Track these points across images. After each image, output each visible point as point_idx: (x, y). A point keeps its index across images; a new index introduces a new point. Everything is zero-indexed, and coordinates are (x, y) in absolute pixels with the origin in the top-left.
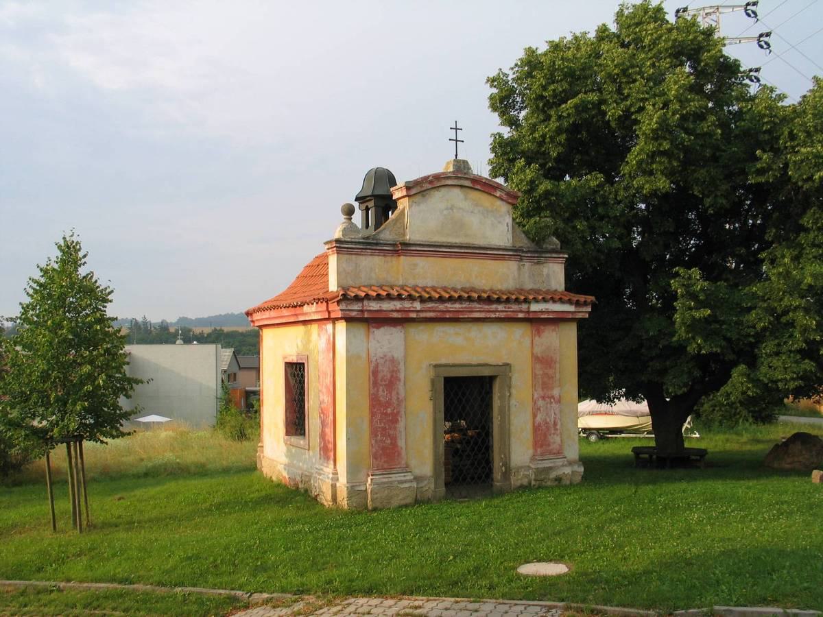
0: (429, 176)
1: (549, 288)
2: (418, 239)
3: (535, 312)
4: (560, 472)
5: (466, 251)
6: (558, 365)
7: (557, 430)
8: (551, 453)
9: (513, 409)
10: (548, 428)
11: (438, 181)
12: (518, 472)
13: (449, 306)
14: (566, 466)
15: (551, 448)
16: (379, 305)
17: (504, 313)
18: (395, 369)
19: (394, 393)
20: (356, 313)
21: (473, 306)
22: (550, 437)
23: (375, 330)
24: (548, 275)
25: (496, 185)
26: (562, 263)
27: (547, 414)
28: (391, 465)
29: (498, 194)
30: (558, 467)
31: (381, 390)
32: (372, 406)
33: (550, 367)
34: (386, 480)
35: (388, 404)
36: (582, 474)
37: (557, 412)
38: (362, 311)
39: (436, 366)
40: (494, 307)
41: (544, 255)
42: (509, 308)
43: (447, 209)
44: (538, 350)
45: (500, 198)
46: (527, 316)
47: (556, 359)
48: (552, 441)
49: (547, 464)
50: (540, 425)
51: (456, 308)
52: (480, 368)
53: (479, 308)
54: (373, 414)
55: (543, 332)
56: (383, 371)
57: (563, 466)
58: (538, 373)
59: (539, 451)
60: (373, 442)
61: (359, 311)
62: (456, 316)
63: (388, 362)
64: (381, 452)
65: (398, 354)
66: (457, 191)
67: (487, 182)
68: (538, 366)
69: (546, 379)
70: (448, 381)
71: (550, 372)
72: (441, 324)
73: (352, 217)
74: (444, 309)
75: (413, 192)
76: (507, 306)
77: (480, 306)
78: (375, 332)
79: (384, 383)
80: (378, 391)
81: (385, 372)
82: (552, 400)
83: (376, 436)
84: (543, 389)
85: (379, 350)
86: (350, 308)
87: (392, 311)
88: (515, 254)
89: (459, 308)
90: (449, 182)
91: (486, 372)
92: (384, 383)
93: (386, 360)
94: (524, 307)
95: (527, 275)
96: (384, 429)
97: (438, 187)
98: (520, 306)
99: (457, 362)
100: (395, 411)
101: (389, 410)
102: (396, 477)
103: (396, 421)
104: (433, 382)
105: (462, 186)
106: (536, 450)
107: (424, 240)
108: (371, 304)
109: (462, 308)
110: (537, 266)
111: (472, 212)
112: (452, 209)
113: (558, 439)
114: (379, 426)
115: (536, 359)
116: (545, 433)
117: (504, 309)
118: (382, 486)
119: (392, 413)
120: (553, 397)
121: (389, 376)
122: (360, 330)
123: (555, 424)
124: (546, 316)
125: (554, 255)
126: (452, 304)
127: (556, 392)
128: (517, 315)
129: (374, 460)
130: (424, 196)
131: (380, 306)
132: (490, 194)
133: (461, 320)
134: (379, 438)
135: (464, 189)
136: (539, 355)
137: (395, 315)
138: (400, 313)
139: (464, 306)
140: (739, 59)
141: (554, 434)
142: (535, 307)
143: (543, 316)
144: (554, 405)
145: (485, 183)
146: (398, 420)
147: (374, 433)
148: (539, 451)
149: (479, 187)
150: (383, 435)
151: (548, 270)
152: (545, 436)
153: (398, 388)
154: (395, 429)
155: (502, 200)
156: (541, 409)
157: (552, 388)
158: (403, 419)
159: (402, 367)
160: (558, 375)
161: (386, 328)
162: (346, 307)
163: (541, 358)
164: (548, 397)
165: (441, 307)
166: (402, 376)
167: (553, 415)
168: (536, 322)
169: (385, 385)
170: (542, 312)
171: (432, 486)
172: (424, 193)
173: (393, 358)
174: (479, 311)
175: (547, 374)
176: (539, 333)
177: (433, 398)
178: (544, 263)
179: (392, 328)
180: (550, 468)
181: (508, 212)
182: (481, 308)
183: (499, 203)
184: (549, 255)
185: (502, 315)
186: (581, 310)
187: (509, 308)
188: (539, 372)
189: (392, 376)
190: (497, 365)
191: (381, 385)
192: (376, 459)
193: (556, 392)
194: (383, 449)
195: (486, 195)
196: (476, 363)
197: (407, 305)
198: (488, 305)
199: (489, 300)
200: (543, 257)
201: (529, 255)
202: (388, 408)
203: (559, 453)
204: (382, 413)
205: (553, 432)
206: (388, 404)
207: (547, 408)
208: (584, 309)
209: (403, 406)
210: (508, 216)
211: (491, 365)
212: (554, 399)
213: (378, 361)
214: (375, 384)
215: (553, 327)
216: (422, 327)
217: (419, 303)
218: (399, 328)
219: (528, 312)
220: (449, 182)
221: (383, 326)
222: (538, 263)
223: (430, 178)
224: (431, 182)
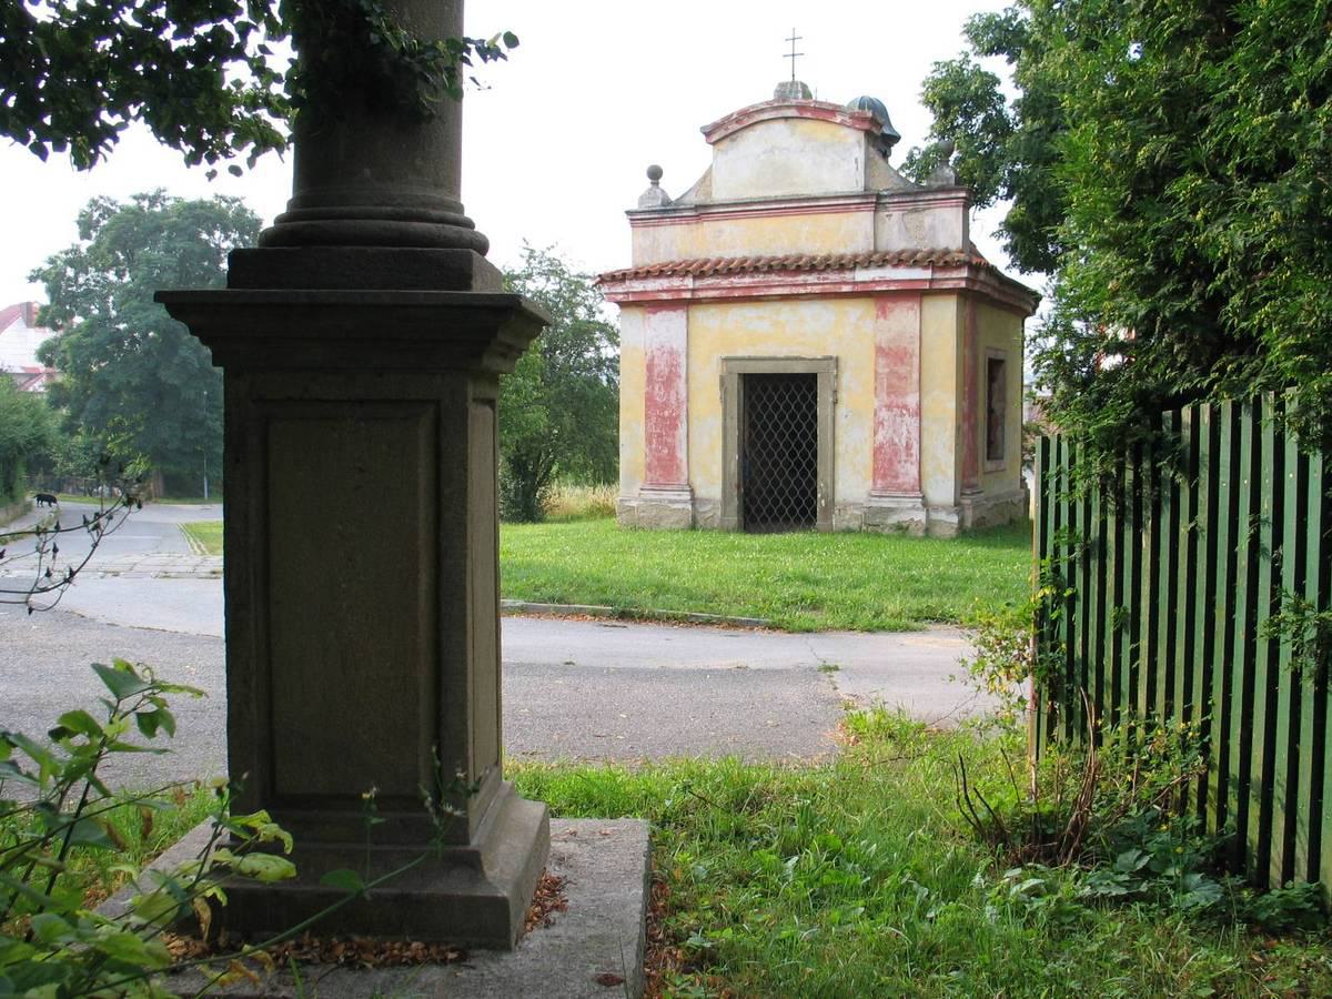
0: (732, 115)
1: (935, 246)
2: (723, 197)
4: (904, 517)
5: (788, 205)
8: (899, 488)
9: (841, 421)
12: (845, 510)
13: (736, 281)
14: (918, 509)
15: (900, 481)
17: (820, 287)
19: (673, 392)
20: (622, 296)
22: (899, 466)
23: (651, 315)
24: (932, 227)
26: (957, 206)
27: (894, 431)
29: (838, 119)
30: (902, 510)
31: (657, 389)
34: (656, 497)
35: (666, 405)
36: (956, 526)
39: (726, 360)
40: (801, 279)
41: (921, 198)
42: (824, 279)
43: (764, 153)
45: (842, 124)
49: (886, 503)
50: (881, 446)
54: (648, 417)
57: (913, 508)
58: (880, 371)
61: (623, 293)
62: (747, 293)
65: (679, 344)
66: (780, 126)
68: (882, 361)
69: (894, 381)
71: (902, 370)
72: (738, 305)
75: (715, 137)
80: (653, 388)
81: (662, 367)
82: (904, 412)
84: (888, 394)
87: (659, 291)
88: (865, 201)
90: (765, 116)
91: (799, 369)
94: (848, 276)
95: (896, 229)
96: (660, 435)
97: (750, 125)
98: (842, 275)
99: (760, 354)
101: (666, 413)
105: (786, 118)
106: (875, 483)
107: (733, 197)
108: (633, 285)
109: (753, 283)
110: (914, 216)
111: (802, 151)
112: (772, 151)
116: (890, 459)
117: (816, 281)
118: (649, 503)
119: (670, 417)
120: (905, 407)
123: (908, 447)
124: (884, 288)
125: (940, 196)
130: (733, 140)
132: (828, 121)
135: (791, 121)
136: (883, 345)
137: (665, 296)
139: (756, 280)
140: (94, 168)
141: (906, 462)
143: (878, 288)
147: (649, 441)
149: (809, 115)
150: (659, 443)
151: (934, 220)
152: (891, 462)
154: (674, 436)
156: (885, 423)
157: (905, 394)
159: (683, 360)
161: (664, 312)
163: (887, 350)
164: (898, 407)
165: (725, 282)
167: (905, 433)
168: (883, 297)
169: (663, 382)
171: (719, 513)
172: (734, 136)
174: (779, 284)
175: (897, 373)
178: (924, 209)
180: (891, 510)
181: (859, 142)
183: (844, 131)
184: (932, 197)
185: (817, 289)
186: (947, 276)
187: (824, 279)
188: (883, 370)
189: (671, 372)
192: (650, 470)
194: (659, 459)
195: (822, 123)
198: (793, 277)
201: (896, 200)
205: (904, 458)
206: (666, 405)
208: (955, 274)
210: (858, 148)
212: (908, 410)
214: (650, 381)
216: (713, 310)
220: (765, 116)
221: (661, 310)
222: (916, 211)
223: (735, 116)
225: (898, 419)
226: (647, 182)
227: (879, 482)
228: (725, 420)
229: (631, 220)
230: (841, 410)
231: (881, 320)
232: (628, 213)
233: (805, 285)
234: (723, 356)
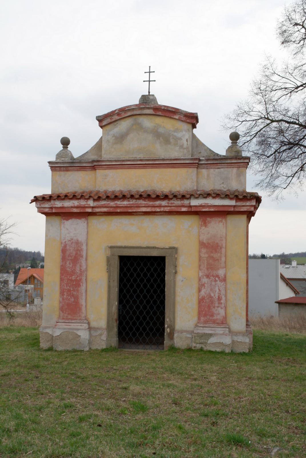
0: (116, 110)
3: (196, 206)
5: (147, 163)
6: (223, 250)
7: (221, 303)
8: (214, 322)
10: (212, 302)
11: (125, 113)
13: (119, 203)
16: (61, 203)
17: (169, 208)
18: (80, 249)
19: (78, 265)
21: (139, 203)
23: (65, 221)
25: (173, 110)
27: (211, 290)
28: (73, 317)
29: (177, 117)
31: (68, 263)
32: (62, 274)
33: (216, 252)
35: (73, 273)
37: (221, 289)
38: (52, 208)
39: (111, 247)
40: (158, 203)
44: (204, 238)
45: (179, 120)
46: (190, 210)
47: (222, 245)
48: (216, 312)
49: (207, 331)
51: (124, 204)
52: (148, 250)
53: (145, 204)
54: (62, 280)
55: (210, 222)
56: (70, 250)
59: (202, 318)
60: (61, 299)
63: (73, 244)
64: (66, 307)
65: (82, 238)
67: (165, 109)
68: (204, 250)
69: (211, 261)
70: (162, 259)
71: (216, 256)
73: (68, 146)
74: (115, 206)
75: (104, 123)
76: (170, 202)
77: (145, 203)
78: (65, 223)
79: (70, 258)
80: (66, 263)
82: (217, 279)
83: (63, 295)
84: (207, 269)
85: (67, 235)
86: (43, 206)
87: (72, 207)
89: (127, 204)
92: (70, 258)
93: (72, 243)
94: (186, 202)
96: (69, 291)
98: (182, 202)
100: (78, 278)
101: (73, 278)
102: (74, 326)
103: (79, 286)
104: (108, 260)
106: (199, 318)
109: (129, 204)
113: (222, 312)
114: (65, 288)
115: (202, 244)
117: (167, 205)
119: (76, 280)
120: (218, 276)
121: (74, 253)
122: (56, 220)
123: (219, 299)
124: (207, 210)
126: (121, 201)
127: (221, 272)
128: (181, 209)
129: (61, 312)
131: (62, 204)
133: (98, 214)
134: (65, 296)
136: (205, 241)
137: (75, 210)
138: (79, 209)
139: (131, 203)
141: (218, 307)
142: (194, 202)
143: (204, 210)
144: (218, 282)
145: (164, 109)
146: (81, 285)
147: (62, 293)
148: (202, 318)
149: (160, 113)
152: (209, 307)
153: (81, 262)
154: (78, 291)
155: (182, 121)
156: (206, 285)
158: (84, 285)
159: (84, 247)
160: (223, 259)
161: (73, 219)
162: (40, 205)
165: (112, 204)
166: (84, 254)
167: (218, 291)
169: (71, 260)
170: (201, 206)
173: (78, 241)
174: (144, 205)
175: (213, 257)
176: (205, 224)
177: (109, 271)
179: (78, 220)
180: (211, 335)
182: (147, 204)
185: (167, 209)
186: (244, 204)
187: (171, 204)
189: (76, 254)
190: (164, 248)
191: (68, 260)
193: (221, 272)
196: (145, 246)
197: (83, 202)
199: (116, 198)
200: (223, 163)
202: (73, 276)
203: (224, 322)
204: (69, 279)
205: (217, 305)
207: (211, 284)
209: (85, 275)
211: (158, 248)
212: (219, 278)
213: (67, 243)
215: (220, 219)
216: (103, 219)
217: (92, 201)
218: (83, 219)
219: (190, 207)
221: (71, 218)
223: (117, 112)
224: (118, 114)
225: (213, 283)
226: (61, 147)
227: (202, 318)
228: (109, 281)
229: (51, 167)
230: (179, 278)
231: (203, 228)
232: (49, 163)
233: (160, 206)
234: (110, 245)
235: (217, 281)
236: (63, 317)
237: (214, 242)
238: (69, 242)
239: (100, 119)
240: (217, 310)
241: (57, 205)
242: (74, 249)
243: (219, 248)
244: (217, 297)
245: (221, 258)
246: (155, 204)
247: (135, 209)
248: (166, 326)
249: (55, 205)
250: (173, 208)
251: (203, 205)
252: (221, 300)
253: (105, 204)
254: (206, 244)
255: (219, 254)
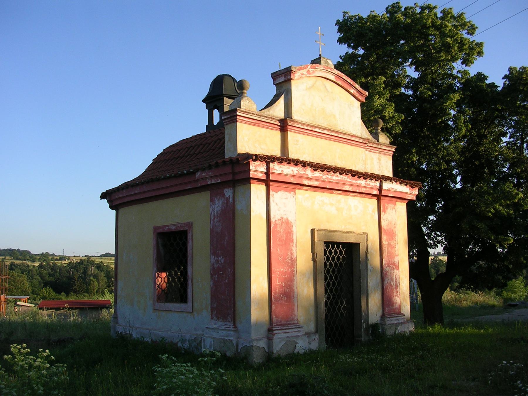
16: (281, 169)
70: (159, 234)
87: (291, 175)
89: (336, 180)
109: (338, 180)
114: (277, 283)
117: (365, 185)
153: (291, 249)
161: (283, 192)
182: (350, 182)
235: (394, 269)
236: (276, 323)
237: (391, 229)
238: (279, 221)
239: (271, 74)
240: (395, 299)
241: (277, 170)
242: (285, 231)
243: (394, 235)
244: (395, 286)
245: (395, 245)
246: (357, 183)
247: (340, 187)
248: (363, 321)
249: (275, 169)
250: (368, 189)
251: (391, 189)
252: (397, 288)
253: (318, 177)
254: (386, 231)
255: (394, 242)
